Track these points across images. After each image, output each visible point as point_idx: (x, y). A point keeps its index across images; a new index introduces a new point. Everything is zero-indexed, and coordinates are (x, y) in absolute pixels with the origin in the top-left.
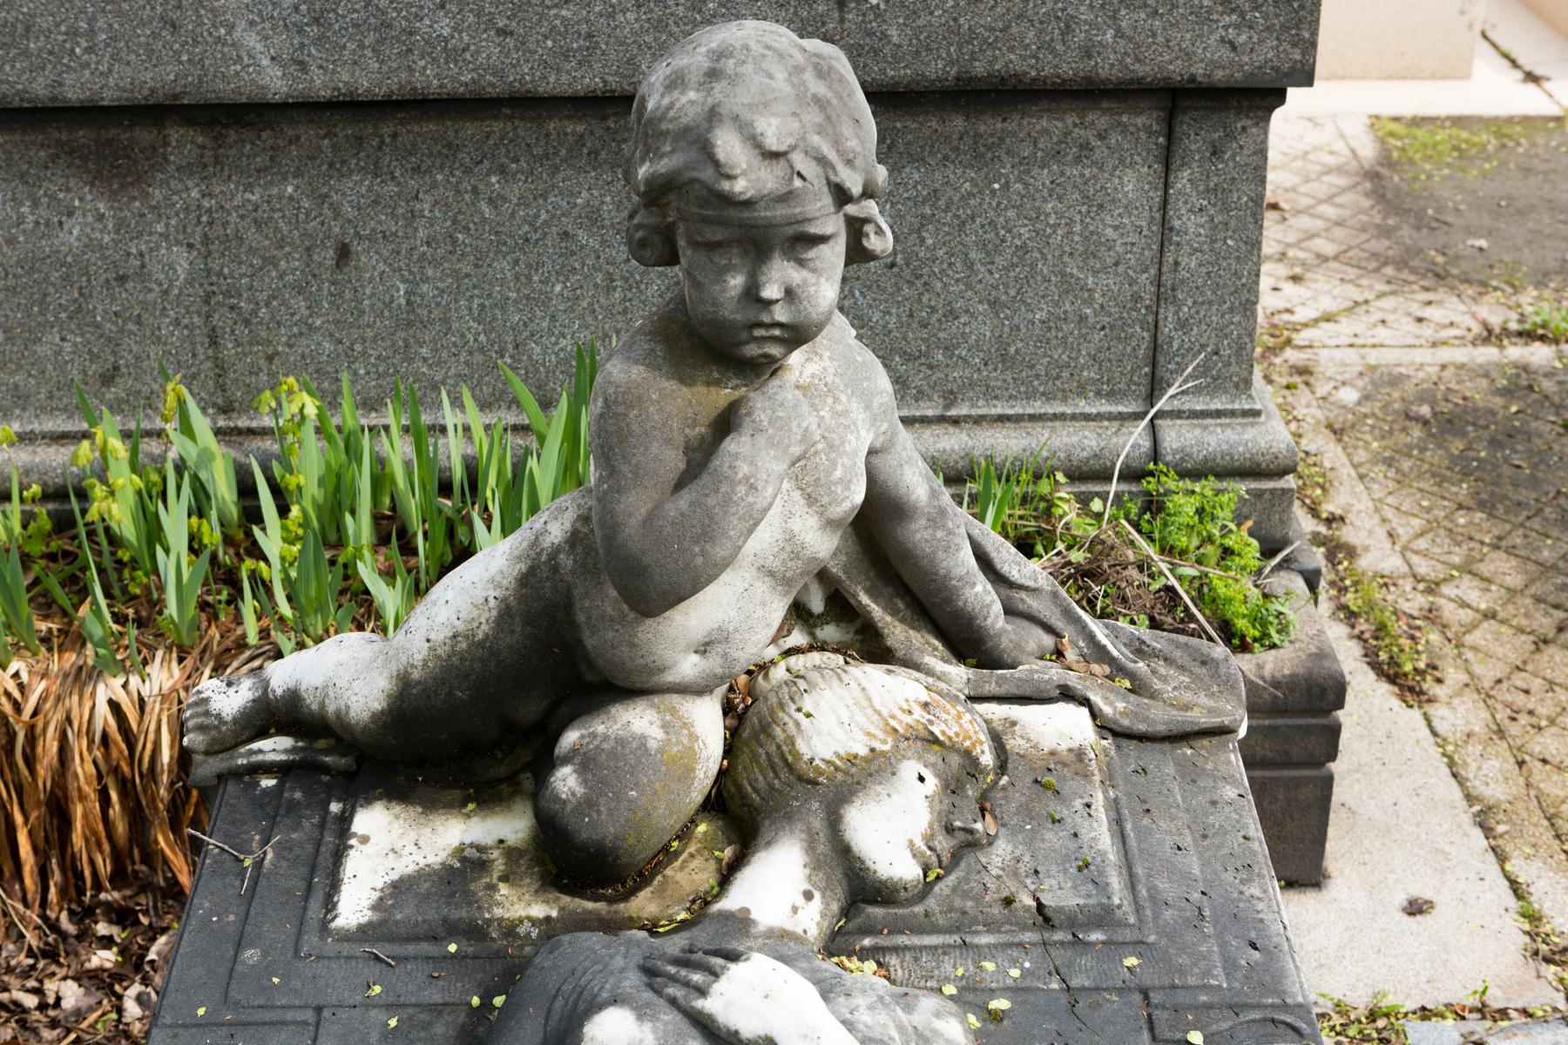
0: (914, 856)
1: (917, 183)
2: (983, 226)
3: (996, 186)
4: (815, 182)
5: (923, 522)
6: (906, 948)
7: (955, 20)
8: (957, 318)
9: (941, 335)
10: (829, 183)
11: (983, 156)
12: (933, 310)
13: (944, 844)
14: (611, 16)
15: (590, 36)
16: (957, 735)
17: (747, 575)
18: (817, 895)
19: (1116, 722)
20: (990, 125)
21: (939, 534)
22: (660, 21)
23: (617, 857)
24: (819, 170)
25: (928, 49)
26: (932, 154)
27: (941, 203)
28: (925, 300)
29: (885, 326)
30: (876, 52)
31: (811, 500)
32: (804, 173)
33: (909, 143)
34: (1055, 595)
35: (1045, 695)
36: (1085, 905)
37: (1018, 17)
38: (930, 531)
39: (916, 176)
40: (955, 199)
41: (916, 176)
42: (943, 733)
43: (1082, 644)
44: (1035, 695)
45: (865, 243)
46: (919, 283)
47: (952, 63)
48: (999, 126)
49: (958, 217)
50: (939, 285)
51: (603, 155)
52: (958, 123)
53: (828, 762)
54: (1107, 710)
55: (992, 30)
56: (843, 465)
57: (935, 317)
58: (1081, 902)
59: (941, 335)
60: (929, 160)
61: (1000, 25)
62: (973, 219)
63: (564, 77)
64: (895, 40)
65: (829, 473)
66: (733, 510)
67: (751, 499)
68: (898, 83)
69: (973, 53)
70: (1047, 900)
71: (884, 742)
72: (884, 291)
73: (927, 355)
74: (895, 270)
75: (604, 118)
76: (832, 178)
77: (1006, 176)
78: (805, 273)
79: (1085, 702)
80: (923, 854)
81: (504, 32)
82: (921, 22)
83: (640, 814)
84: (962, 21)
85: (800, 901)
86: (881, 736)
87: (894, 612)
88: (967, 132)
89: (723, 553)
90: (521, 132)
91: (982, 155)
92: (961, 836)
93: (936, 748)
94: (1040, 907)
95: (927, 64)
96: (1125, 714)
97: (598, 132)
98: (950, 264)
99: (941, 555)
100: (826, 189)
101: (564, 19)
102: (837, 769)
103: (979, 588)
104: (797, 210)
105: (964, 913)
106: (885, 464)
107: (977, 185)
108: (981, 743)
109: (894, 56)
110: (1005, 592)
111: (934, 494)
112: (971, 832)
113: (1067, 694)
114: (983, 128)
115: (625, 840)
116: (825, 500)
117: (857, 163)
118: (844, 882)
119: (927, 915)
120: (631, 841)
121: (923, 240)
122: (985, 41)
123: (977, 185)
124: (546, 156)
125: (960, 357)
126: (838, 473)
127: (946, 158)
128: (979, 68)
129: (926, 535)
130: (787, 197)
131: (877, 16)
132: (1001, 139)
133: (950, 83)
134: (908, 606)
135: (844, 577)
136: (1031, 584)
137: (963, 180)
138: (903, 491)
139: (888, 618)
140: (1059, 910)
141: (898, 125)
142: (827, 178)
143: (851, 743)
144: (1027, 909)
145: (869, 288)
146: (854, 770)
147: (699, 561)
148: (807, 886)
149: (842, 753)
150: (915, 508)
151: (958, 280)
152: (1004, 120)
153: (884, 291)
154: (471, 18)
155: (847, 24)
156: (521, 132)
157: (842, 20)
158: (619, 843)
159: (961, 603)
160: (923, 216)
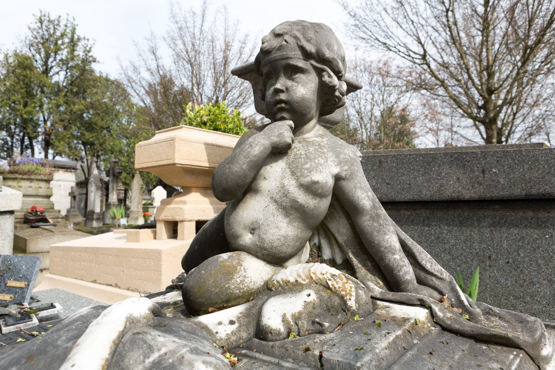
0: (283, 321)
1: (516, 234)
2: (543, 251)
3: (547, 236)
4: (292, 44)
5: (368, 217)
6: (255, 358)
7: (523, 175)
8: (534, 285)
9: (529, 291)
10: (298, 45)
11: (541, 225)
12: (525, 281)
13: (305, 324)
14: (415, 178)
15: (410, 184)
16: (339, 287)
17: (266, 200)
18: (237, 325)
19: (443, 321)
20: (543, 215)
21: (375, 224)
22: (429, 179)
23: (190, 296)
24: (295, 41)
25: (514, 185)
26: (521, 224)
27: (526, 241)
28: (521, 276)
29: (506, 285)
30: (496, 187)
31: (293, 173)
32: (287, 40)
33: (512, 220)
34: (451, 282)
35: (411, 302)
36: (341, 362)
37: (548, 173)
38: (371, 222)
39: (516, 232)
40: (531, 240)
41: (516, 232)
42: (333, 285)
43: (453, 300)
44: (406, 302)
45: (323, 79)
46: (519, 270)
47: (523, 190)
48: (547, 215)
49: (532, 247)
50: (527, 272)
51: (415, 221)
52: (530, 214)
53: (278, 282)
54: (440, 314)
55: (538, 178)
56: (311, 165)
57: (526, 283)
58: (340, 359)
59: (529, 291)
60: (520, 226)
61: (541, 176)
62: (539, 248)
63: (403, 196)
64: (502, 182)
65: (303, 165)
66: (242, 153)
67: (249, 150)
68: (504, 197)
69: (531, 186)
70: (324, 355)
71: (304, 280)
72: (505, 271)
73: (523, 297)
74: (509, 264)
75: (415, 210)
76: (299, 43)
77: (551, 233)
78: (294, 83)
79: (430, 308)
80: (288, 323)
81: (388, 184)
82: (511, 177)
83: (202, 280)
84: (526, 175)
85: (227, 322)
86: (304, 277)
87: (364, 265)
88: (534, 217)
89: (236, 169)
90: (394, 214)
91: (540, 225)
92: (318, 326)
93: (329, 291)
94: (321, 356)
95: (514, 190)
96: (450, 319)
97: (414, 214)
98: (531, 264)
99: (375, 233)
100: (297, 48)
101: (403, 180)
102: (280, 285)
103: (397, 257)
104: (284, 53)
105: (287, 350)
106: (348, 186)
107: (539, 236)
108: (351, 295)
109: (502, 188)
110: (418, 271)
111: (374, 207)
112: (321, 325)
113: (422, 304)
114: (540, 216)
115: (193, 289)
116: (299, 174)
117: (312, 41)
118: (255, 327)
119: (272, 347)
120: (196, 290)
121: (519, 255)
122: (535, 182)
123: (539, 236)
124: (400, 221)
125: (537, 300)
126: (307, 166)
127: (526, 225)
128: (534, 191)
129: (370, 223)
130: (281, 48)
131: (496, 175)
132: (548, 220)
133: (523, 197)
134: (372, 266)
135: (344, 245)
136: (439, 274)
137: (535, 234)
138: (356, 199)
139: (360, 266)
140: (328, 361)
141: (508, 214)
142: (297, 44)
143: (290, 277)
144: (314, 356)
145: (500, 270)
146: (286, 287)
147: (227, 171)
148: (234, 319)
149: (284, 279)
150: (363, 210)
151: (534, 270)
152: (549, 213)
153: (505, 271)
154: (380, 180)
155: (486, 178)
156: (394, 214)
157: (484, 177)
158: (191, 289)
159: (387, 261)
160: (519, 246)
